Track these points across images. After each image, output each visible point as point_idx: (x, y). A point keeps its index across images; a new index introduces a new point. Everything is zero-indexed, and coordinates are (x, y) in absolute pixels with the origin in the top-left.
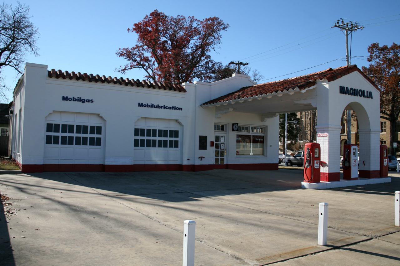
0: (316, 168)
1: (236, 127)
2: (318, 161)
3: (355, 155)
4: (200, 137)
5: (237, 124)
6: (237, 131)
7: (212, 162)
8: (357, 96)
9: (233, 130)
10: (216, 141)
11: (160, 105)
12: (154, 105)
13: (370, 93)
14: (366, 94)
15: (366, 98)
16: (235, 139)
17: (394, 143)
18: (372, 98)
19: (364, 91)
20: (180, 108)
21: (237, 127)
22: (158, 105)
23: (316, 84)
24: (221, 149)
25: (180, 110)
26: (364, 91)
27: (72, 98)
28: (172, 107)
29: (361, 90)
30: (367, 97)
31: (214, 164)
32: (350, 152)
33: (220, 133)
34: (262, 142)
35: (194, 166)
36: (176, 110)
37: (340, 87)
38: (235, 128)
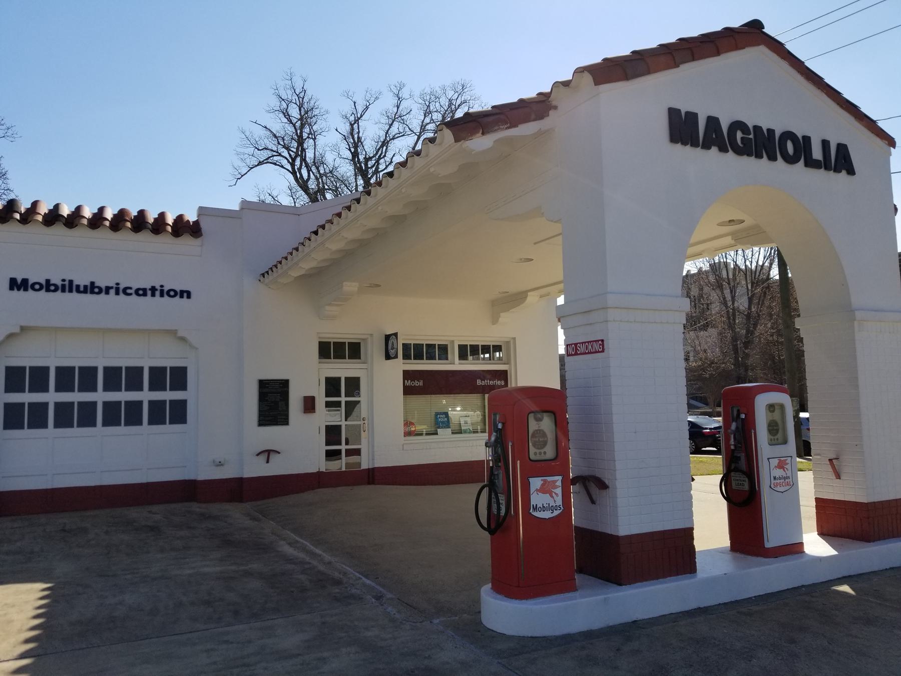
3: (779, 436)
4: (263, 385)
11: (102, 283)
12: (75, 283)
13: (842, 149)
15: (820, 175)
18: (851, 171)
19: (807, 140)
20: (182, 292)
22: (92, 283)
23: (551, 112)
25: (182, 297)
26: (807, 140)
27: (44, 283)
28: (148, 287)
29: (788, 135)
30: (825, 164)
33: (342, 369)
35: (240, 480)
36: (166, 296)
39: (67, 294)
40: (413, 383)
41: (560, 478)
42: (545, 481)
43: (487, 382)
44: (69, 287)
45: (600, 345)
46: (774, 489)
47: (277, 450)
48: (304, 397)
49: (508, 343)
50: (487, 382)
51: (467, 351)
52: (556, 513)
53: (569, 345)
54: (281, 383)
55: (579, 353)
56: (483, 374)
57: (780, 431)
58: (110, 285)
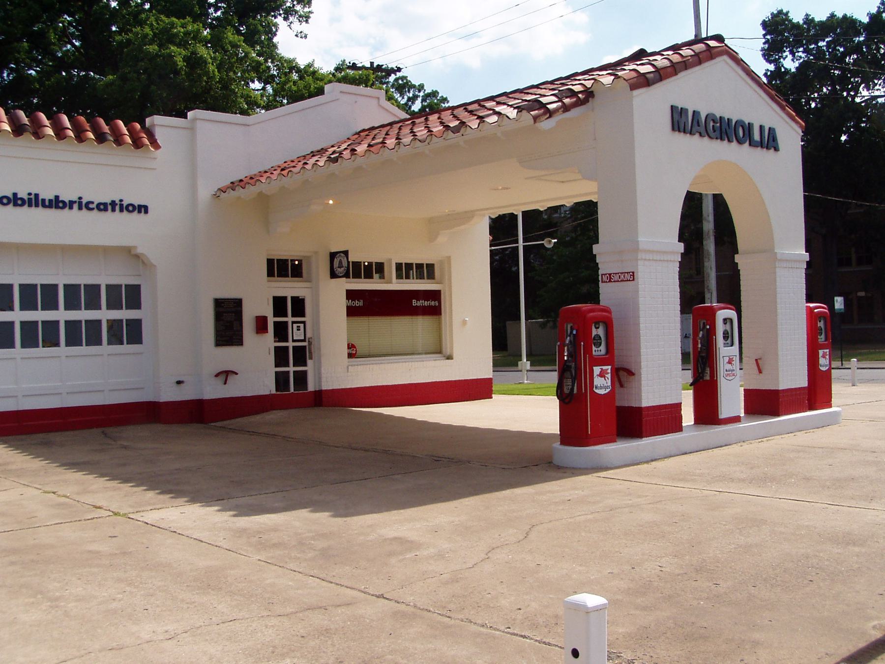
0: (597, 391)
1: (340, 262)
2: (604, 368)
3: (729, 341)
4: (219, 303)
5: (346, 253)
6: (347, 275)
7: (266, 385)
8: (730, 141)
9: (333, 275)
10: (276, 315)
11: (65, 197)
12: (41, 197)
14: (757, 137)
16: (342, 303)
17: (836, 298)
18: (776, 149)
20: (140, 207)
21: (345, 264)
22: (57, 197)
24: (294, 341)
25: (140, 212)
27: (11, 196)
28: (109, 201)
29: (740, 123)
30: (761, 144)
31: (274, 392)
32: (712, 332)
33: (289, 288)
34: (435, 311)
36: (125, 212)
37: (673, 108)
38: (340, 266)
39: (33, 209)
40: (354, 303)
41: (609, 367)
42: (823, 352)
43: (422, 303)
44: (34, 201)
45: (631, 275)
46: (727, 378)
47: (234, 371)
48: (256, 317)
49: (441, 262)
50: (422, 303)
51: (404, 270)
52: (608, 390)
53: (604, 274)
54: (234, 303)
55: (612, 281)
56: (416, 294)
57: (730, 339)
58: (74, 200)
